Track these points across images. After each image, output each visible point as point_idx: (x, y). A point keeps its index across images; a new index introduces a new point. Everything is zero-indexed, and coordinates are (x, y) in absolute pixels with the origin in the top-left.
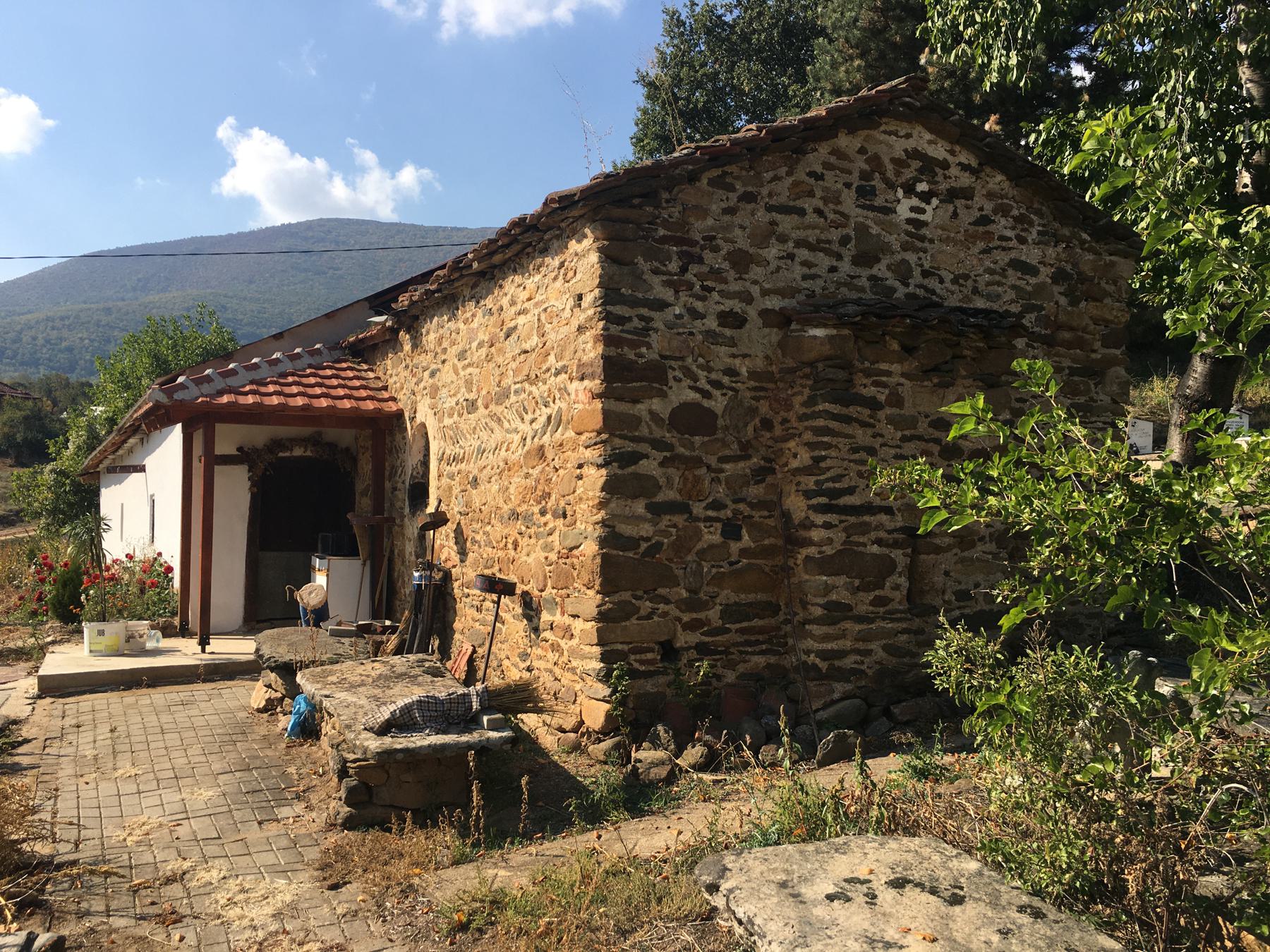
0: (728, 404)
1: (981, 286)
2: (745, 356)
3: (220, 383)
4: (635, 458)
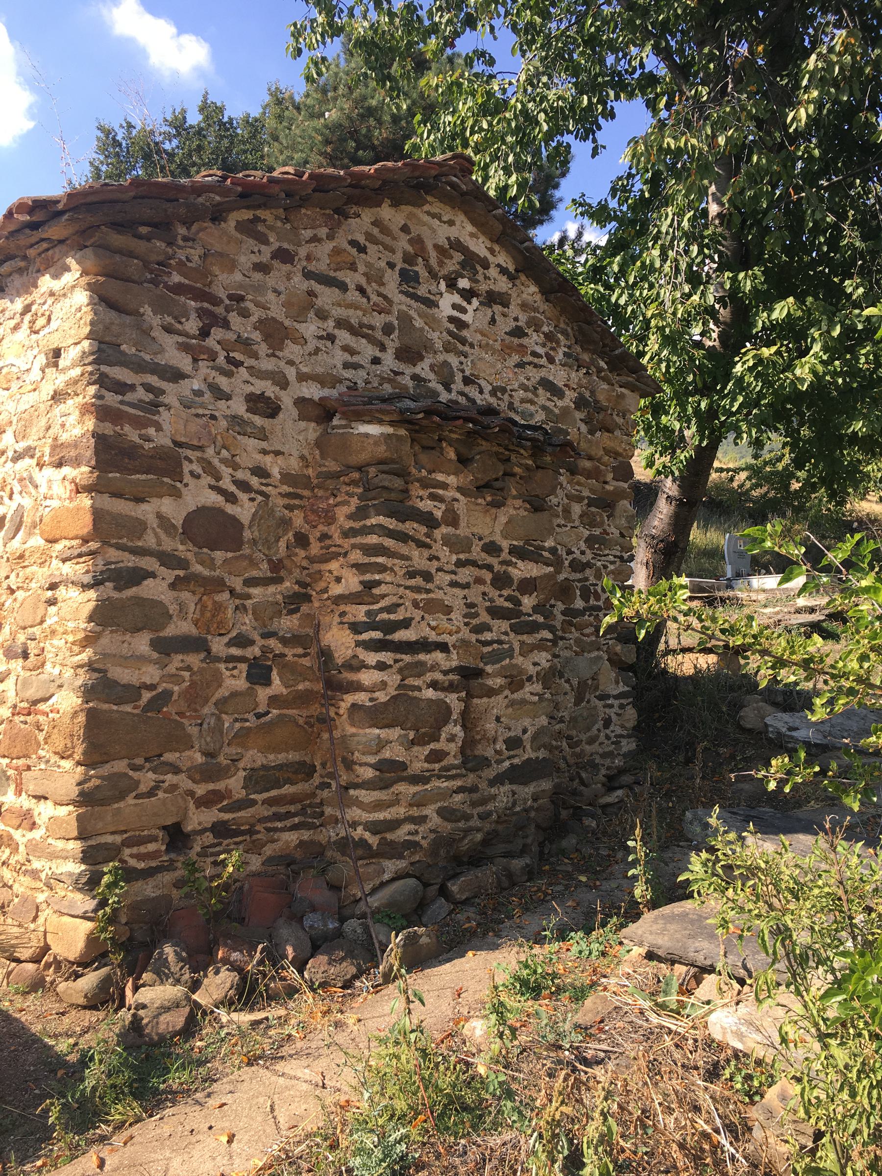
0: (256, 512)
1: (517, 404)
2: (277, 453)
4: (137, 576)
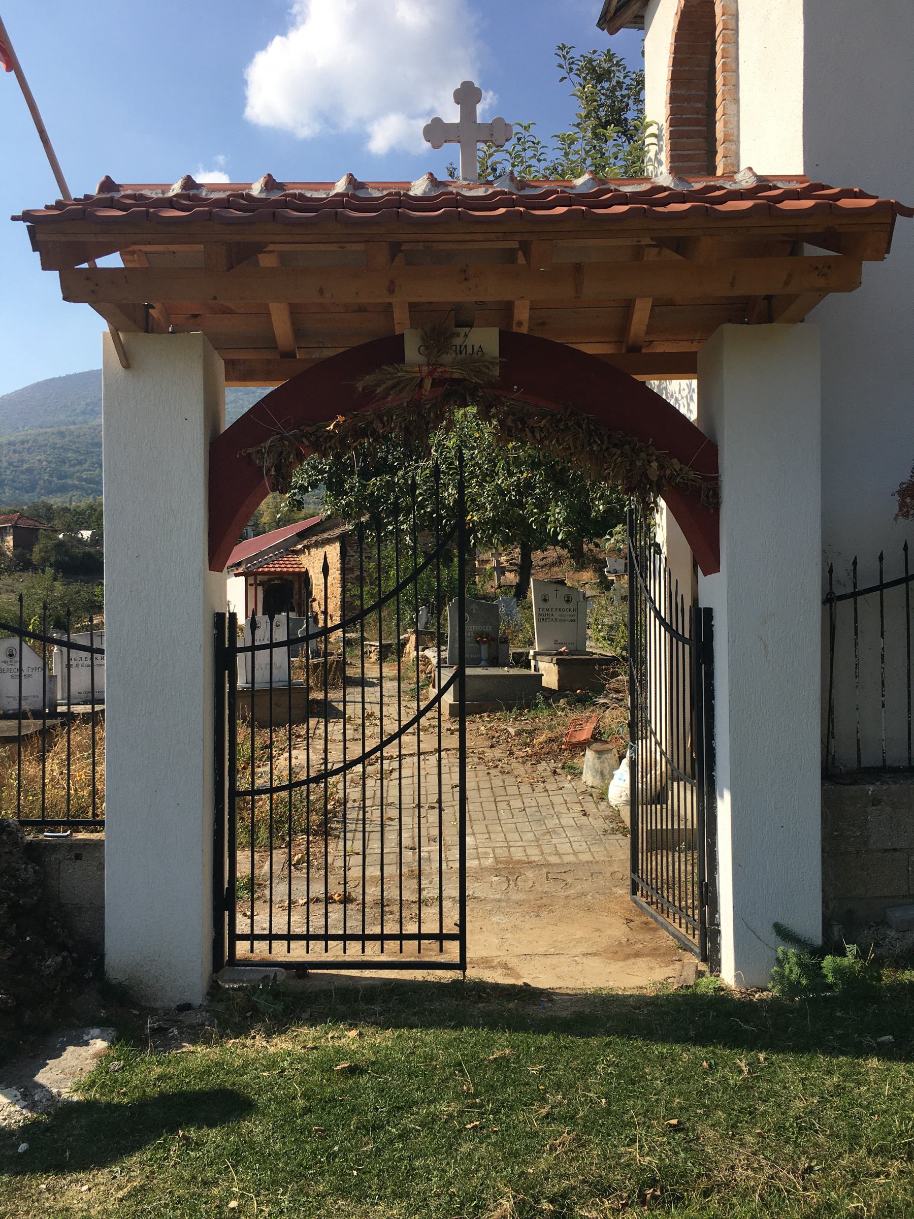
3: (258, 565)
